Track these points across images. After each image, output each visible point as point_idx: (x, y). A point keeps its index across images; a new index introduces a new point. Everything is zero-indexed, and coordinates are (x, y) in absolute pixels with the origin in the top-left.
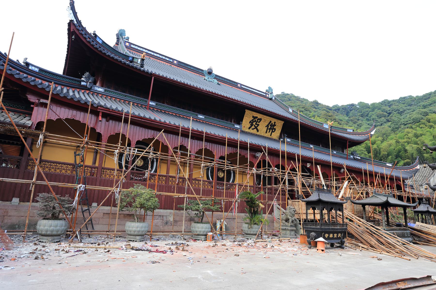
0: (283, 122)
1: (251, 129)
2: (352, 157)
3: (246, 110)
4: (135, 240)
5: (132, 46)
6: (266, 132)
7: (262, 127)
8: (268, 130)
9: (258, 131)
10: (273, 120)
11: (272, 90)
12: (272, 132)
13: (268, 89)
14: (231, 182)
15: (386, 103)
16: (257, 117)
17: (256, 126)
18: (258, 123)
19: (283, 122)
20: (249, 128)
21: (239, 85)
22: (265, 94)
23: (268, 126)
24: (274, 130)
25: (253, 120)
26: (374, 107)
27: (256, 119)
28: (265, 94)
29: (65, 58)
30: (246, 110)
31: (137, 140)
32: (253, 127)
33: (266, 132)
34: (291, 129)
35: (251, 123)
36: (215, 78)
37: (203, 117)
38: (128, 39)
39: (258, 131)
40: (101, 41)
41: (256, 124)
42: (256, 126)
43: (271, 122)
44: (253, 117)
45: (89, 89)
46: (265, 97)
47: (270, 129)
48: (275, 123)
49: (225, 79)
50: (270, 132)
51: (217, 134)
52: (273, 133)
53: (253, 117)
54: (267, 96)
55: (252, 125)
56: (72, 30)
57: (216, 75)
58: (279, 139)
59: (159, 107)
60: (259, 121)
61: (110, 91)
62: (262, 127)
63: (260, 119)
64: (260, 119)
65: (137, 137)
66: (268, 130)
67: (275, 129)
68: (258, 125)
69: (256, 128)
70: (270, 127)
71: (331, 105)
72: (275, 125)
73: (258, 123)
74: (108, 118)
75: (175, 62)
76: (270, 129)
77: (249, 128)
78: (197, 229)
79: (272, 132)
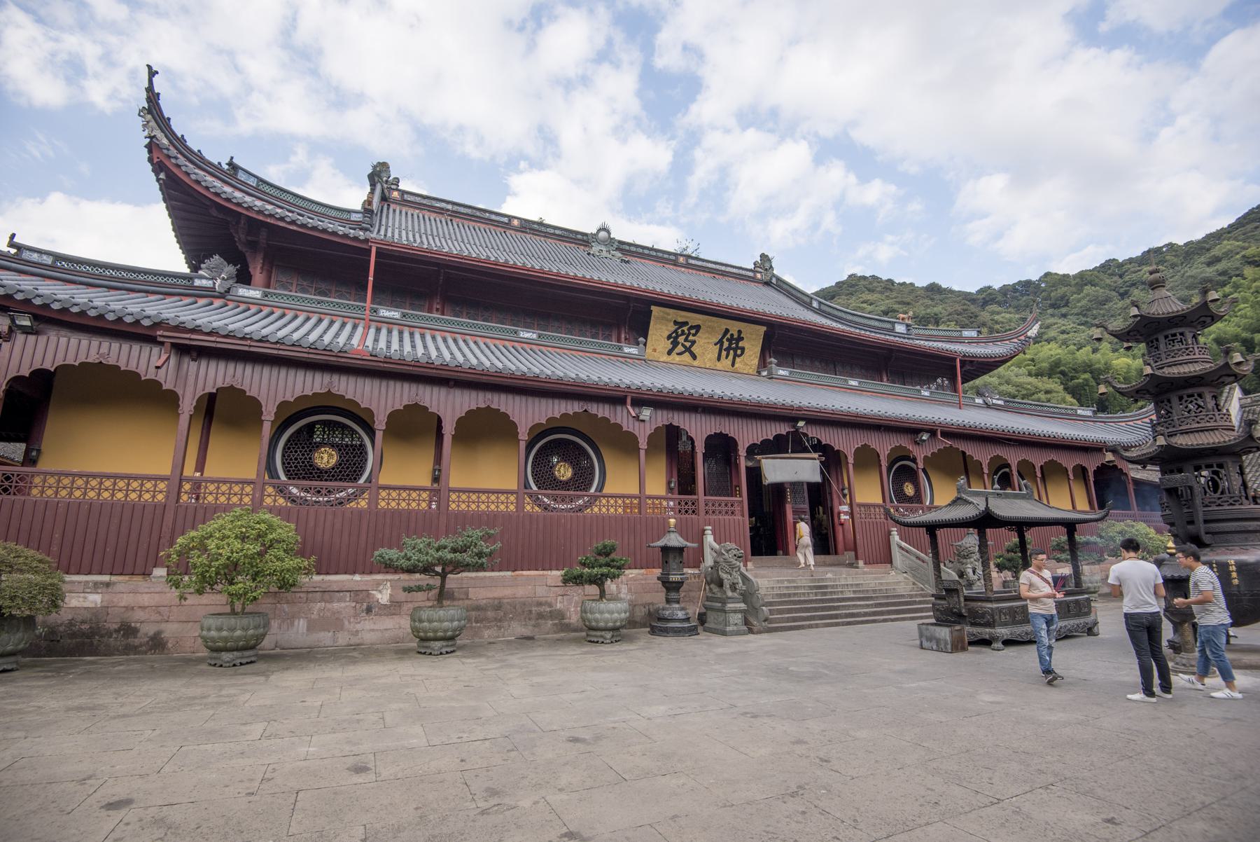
0: (765, 328)
1: (674, 353)
2: (979, 401)
3: (653, 308)
4: (219, 663)
5: (691, 261)
6: (719, 359)
7: (706, 345)
8: (724, 353)
9: (694, 357)
10: (734, 327)
11: (769, 260)
12: (736, 355)
13: (758, 259)
14: (592, 490)
15: (1109, 267)
16: (686, 323)
17: (688, 344)
18: (691, 338)
19: (765, 328)
20: (669, 353)
21: (681, 260)
22: (751, 274)
23: (720, 342)
24: (739, 352)
25: (676, 331)
26: (1084, 279)
27: (685, 329)
28: (751, 274)
29: (171, 235)
30: (653, 308)
31: (280, 400)
32: (680, 348)
33: (719, 359)
34: (789, 344)
35: (674, 339)
36: (617, 249)
37: (535, 336)
38: (397, 180)
39: (694, 357)
40: (252, 179)
41: (686, 340)
42: (688, 344)
43: (727, 331)
44: (676, 323)
45: (222, 296)
46: (753, 280)
47: (728, 350)
48: (740, 332)
49: (577, 233)
50: (731, 357)
51: (583, 376)
52: (738, 359)
53: (676, 323)
54: (759, 276)
55: (675, 344)
56: (156, 160)
57: (620, 242)
58: (759, 373)
59: (797, 378)
60: (693, 331)
61: (418, 317)
62: (706, 345)
63: (698, 328)
64: (698, 328)
65: (390, 402)
66: (724, 353)
67: (743, 349)
68: (693, 342)
69: (688, 350)
70: (726, 344)
71: (973, 289)
72: (742, 339)
73: (691, 338)
74: (195, 354)
75: (516, 222)
76: (728, 350)
77: (669, 353)
78: (597, 615)
79: (736, 355)
